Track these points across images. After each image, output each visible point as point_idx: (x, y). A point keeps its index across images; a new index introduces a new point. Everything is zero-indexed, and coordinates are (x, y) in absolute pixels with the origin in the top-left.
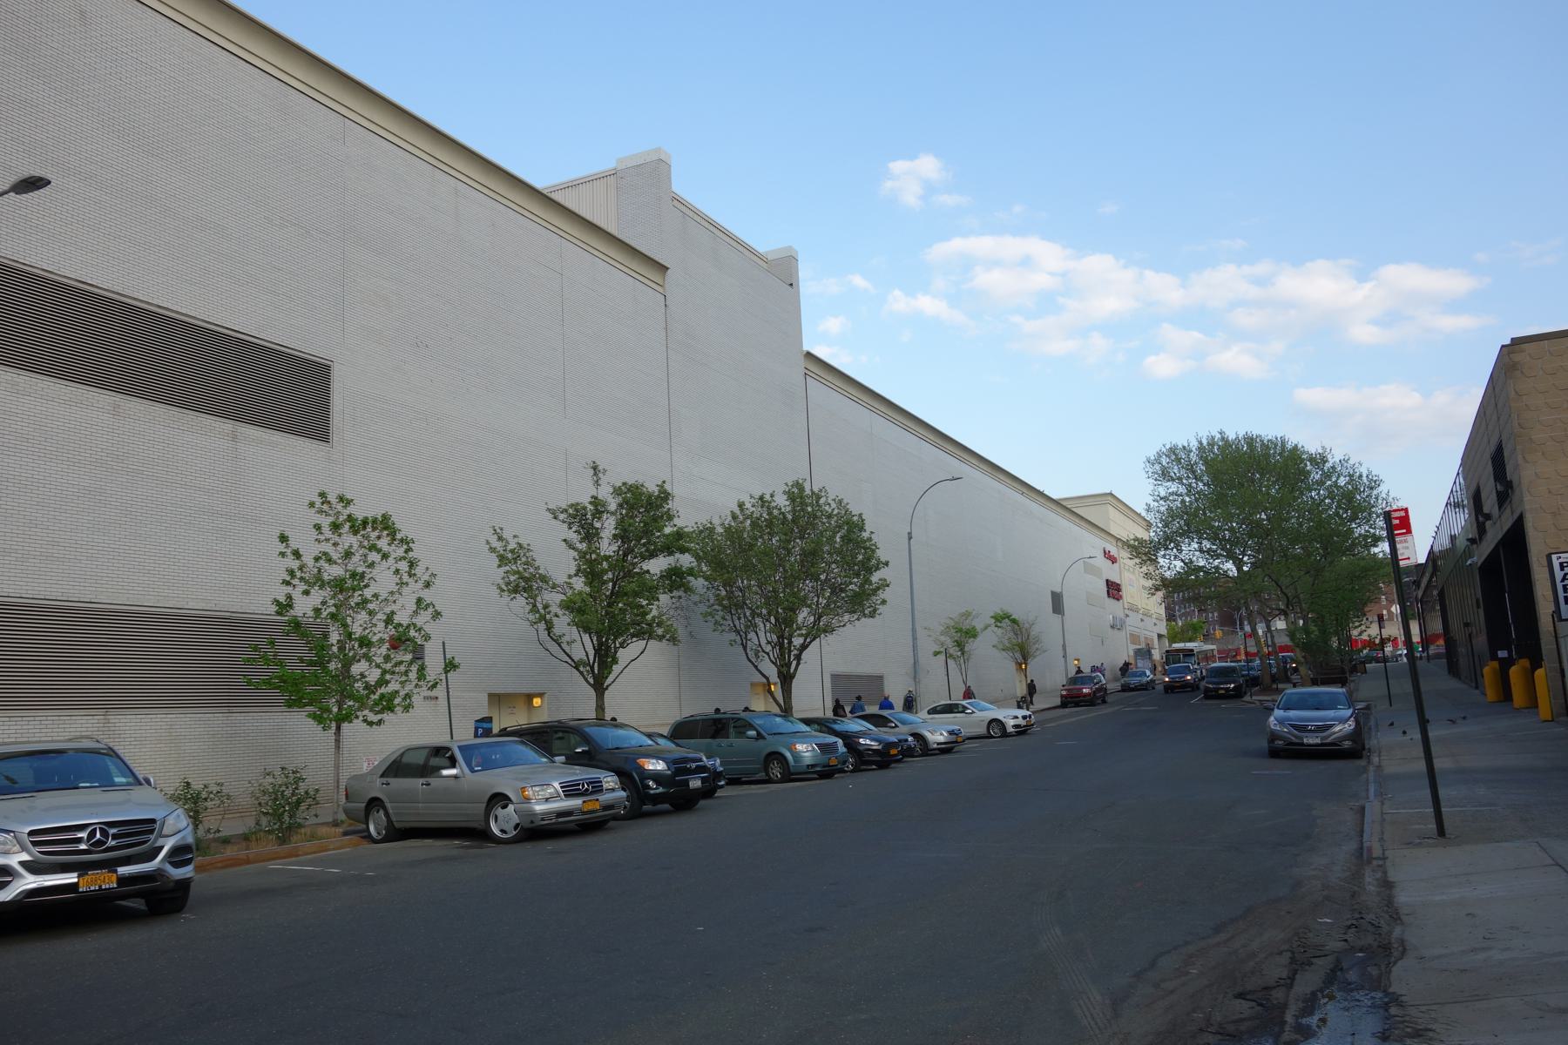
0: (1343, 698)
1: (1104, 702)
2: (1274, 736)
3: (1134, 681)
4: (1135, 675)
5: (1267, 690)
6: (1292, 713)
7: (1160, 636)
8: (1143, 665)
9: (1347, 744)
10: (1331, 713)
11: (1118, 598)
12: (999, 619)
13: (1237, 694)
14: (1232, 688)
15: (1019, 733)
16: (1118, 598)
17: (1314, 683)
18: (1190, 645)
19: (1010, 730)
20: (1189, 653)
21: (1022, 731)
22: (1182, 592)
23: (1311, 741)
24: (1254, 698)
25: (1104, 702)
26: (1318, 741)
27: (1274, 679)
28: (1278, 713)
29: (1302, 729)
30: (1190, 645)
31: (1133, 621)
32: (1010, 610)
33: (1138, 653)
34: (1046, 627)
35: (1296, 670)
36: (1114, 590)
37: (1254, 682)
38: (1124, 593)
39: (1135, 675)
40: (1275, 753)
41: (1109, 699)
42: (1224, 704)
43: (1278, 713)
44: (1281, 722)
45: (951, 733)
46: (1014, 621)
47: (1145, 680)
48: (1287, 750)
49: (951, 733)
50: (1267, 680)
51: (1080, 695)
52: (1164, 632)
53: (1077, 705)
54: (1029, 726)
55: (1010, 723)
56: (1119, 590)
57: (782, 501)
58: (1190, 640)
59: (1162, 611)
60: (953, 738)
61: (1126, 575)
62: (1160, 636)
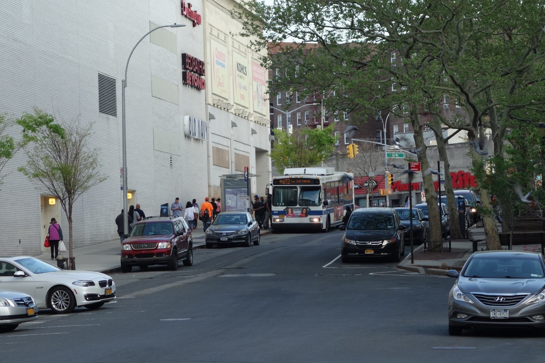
0: (538, 264)
1: (187, 263)
2: (457, 309)
3: (227, 230)
4: (228, 220)
5: (436, 251)
6: (479, 282)
7: (260, 152)
8: (238, 204)
9: (538, 319)
10: (524, 283)
11: (199, 86)
12: (31, 124)
13: (392, 256)
14: (377, 246)
15: (90, 308)
16: (199, 86)
17: (505, 241)
18: (313, 172)
19: (82, 301)
20: (312, 185)
21: (96, 304)
22: (294, 76)
23: (499, 315)
24: (416, 263)
25: (187, 263)
26: (506, 315)
27: (446, 234)
28: (463, 281)
29: (489, 300)
30: (313, 172)
31: (220, 125)
32: (48, 110)
33: (229, 182)
34: (100, 138)
35: (476, 218)
36: (193, 71)
37: (415, 237)
38: (208, 77)
39: (228, 220)
40: (456, 330)
41: (195, 259)
42: (373, 272)
43: (463, 281)
44: (465, 292)
45: (19, 302)
46: (56, 130)
47: (244, 229)
48: (470, 326)
49: (19, 302)
50: (436, 234)
51: (147, 250)
52: (266, 146)
53: (144, 268)
54: (108, 296)
55: (82, 293)
56: (201, 72)
57: (348, 151)
58: (312, 162)
59: (265, 109)
60: (22, 310)
61: (214, 46)
62: (260, 152)
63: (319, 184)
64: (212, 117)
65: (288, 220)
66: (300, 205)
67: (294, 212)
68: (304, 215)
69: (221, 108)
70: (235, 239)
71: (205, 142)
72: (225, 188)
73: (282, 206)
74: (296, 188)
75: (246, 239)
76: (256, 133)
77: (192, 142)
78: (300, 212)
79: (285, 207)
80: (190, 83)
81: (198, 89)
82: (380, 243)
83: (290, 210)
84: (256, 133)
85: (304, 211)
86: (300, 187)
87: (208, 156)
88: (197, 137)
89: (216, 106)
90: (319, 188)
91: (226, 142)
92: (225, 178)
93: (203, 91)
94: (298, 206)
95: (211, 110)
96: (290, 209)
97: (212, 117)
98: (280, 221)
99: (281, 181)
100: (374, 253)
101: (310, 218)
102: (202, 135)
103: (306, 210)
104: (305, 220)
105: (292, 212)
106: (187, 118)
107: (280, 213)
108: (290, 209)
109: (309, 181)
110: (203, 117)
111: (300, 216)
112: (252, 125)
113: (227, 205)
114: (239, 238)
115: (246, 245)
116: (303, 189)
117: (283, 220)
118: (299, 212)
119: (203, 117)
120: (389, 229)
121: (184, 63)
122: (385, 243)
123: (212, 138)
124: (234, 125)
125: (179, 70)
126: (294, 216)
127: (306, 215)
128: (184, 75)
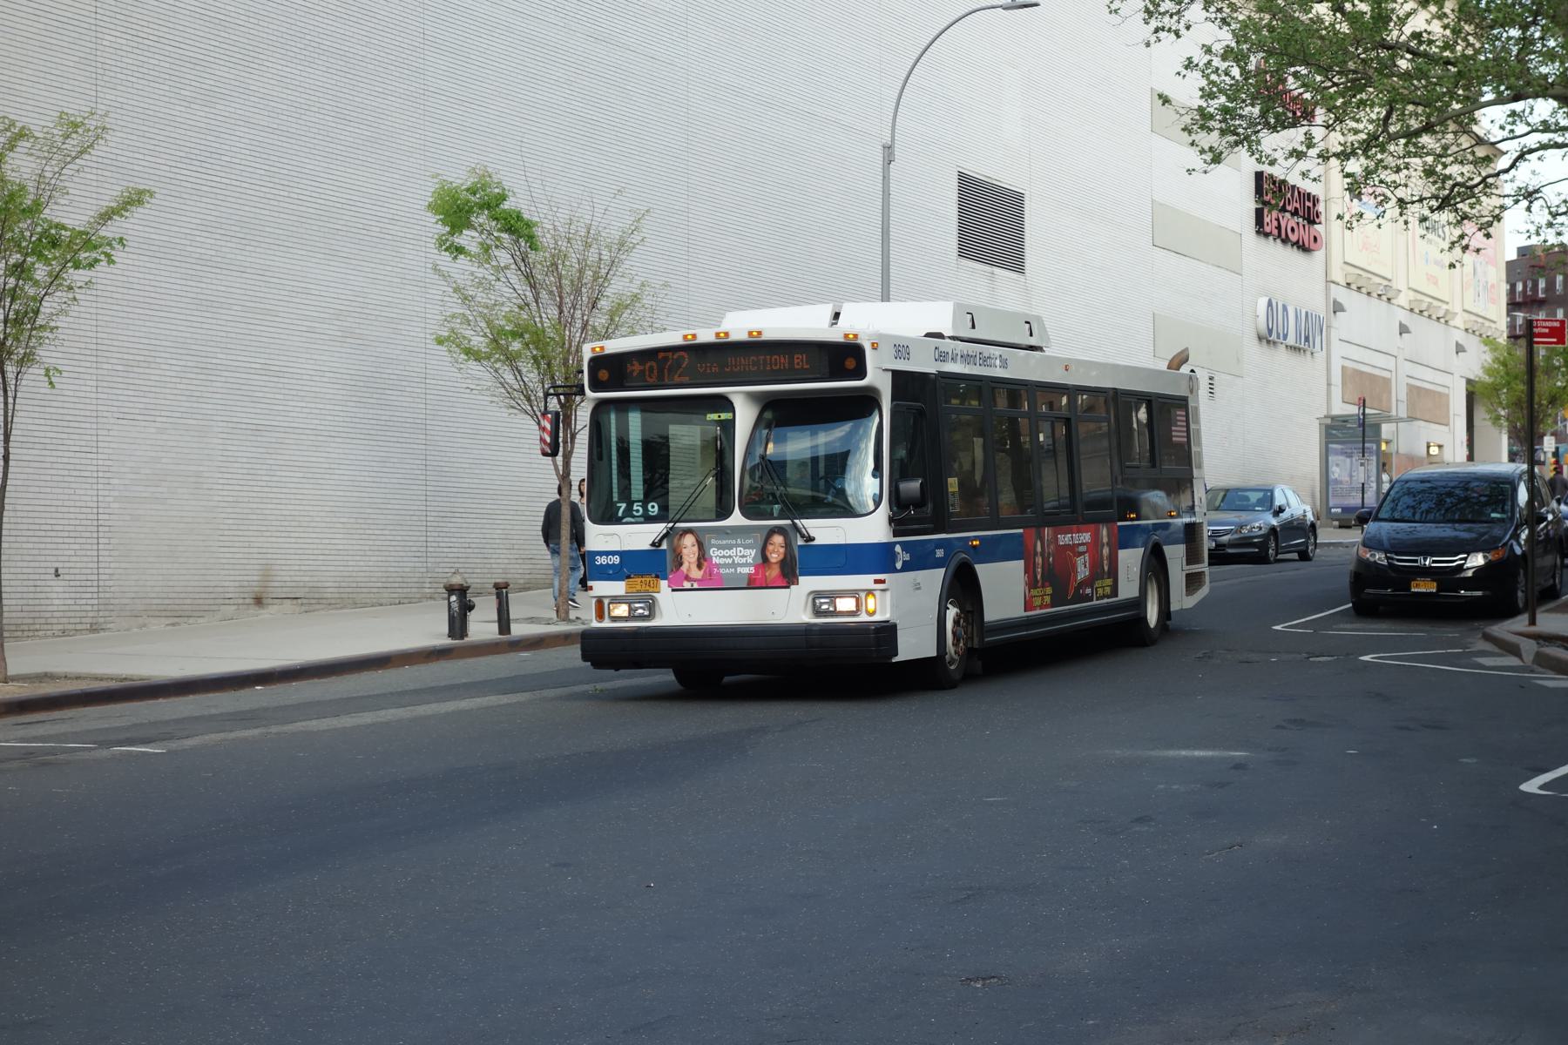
56: (1312, 219)
63: (860, 372)
64: (1338, 308)
65: (680, 609)
66: (746, 514)
67: (716, 555)
68: (774, 572)
69: (1369, 294)
70: (1232, 545)
71: (1320, 356)
72: (1327, 443)
73: (649, 519)
74: (724, 403)
75: (1263, 546)
76: (1408, 331)
77: (1281, 354)
78: (751, 555)
79: (659, 528)
80: (1275, 232)
81: (1303, 248)
82: (1457, 560)
83: (688, 544)
84: (1408, 331)
85: (776, 554)
86: (753, 396)
87: (1329, 385)
88: (1291, 340)
89: (1354, 287)
90: (864, 403)
91: (1380, 360)
92: (1329, 421)
93: (1319, 255)
94: (736, 519)
96: (689, 540)
97: (1338, 308)
98: (631, 617)
99: (636, 367)
100: (1439, 590)
101: (817, 595)
102: (1307, 339)
103: (788, 545)
104: (787, 607)
105: (702, 559)
106: (1263, 302)
107: (632, 565)
108: (689, 540)
109: (800, 360)
110: (1319, 307)
111: (753, 584)
112: (1459, 336)
113: (1332, 477)
114: (1246, 542)
115: (1260, 558)
116: (781, 414)
117: (652, 607)
118: (739, 557)
119: (1319, 307)
120: (1494, 521)
121: (1259, 190)
122: (1478, 560)
124: (1404, 329)
125: (1250, 205)
126: (713, 582)
127: (789, 574)
128: (1259, 215)
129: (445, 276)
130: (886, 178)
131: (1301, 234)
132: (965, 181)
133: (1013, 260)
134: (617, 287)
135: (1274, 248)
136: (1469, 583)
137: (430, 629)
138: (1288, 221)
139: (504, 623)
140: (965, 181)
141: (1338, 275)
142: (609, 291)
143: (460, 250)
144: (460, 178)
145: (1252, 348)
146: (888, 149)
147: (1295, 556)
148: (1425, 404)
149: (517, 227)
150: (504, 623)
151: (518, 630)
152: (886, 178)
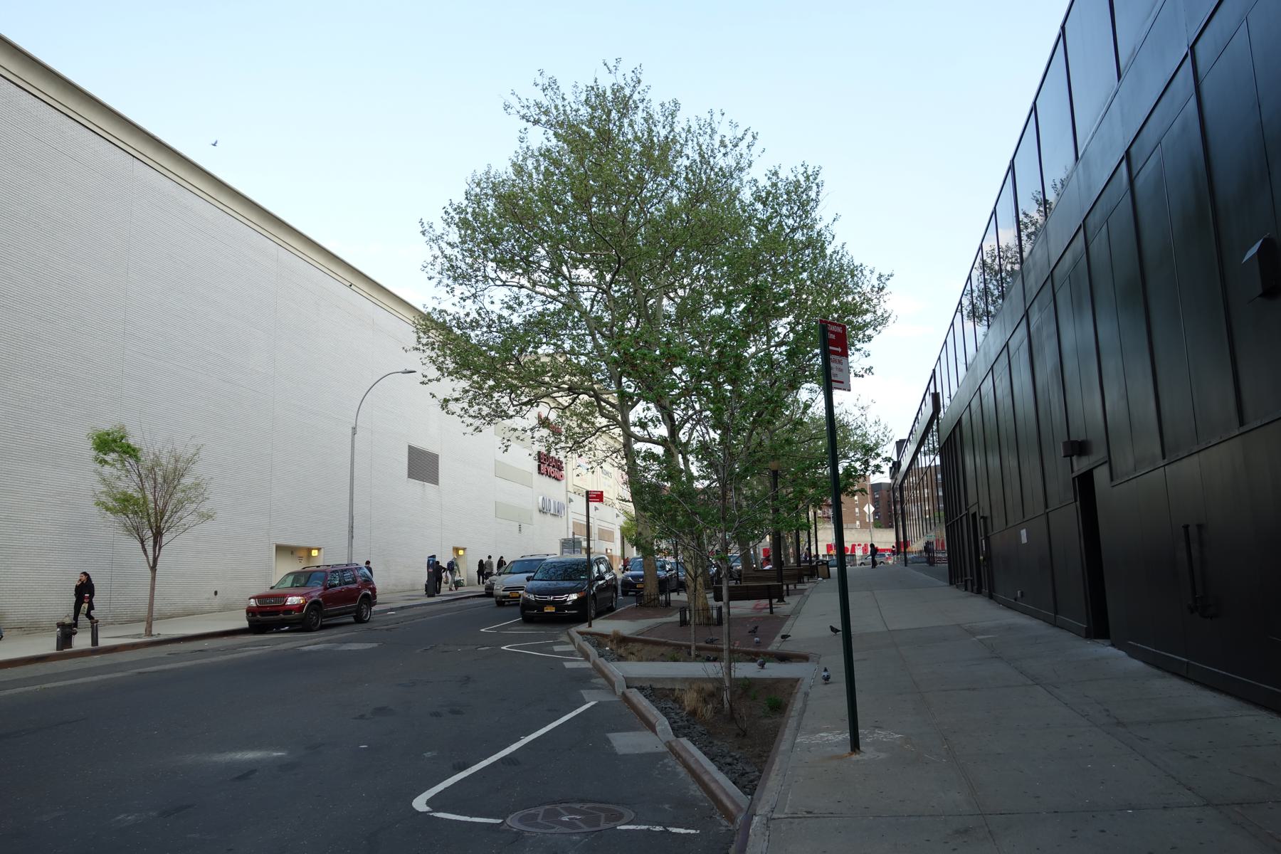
56: (560, 469)
64: (571, 501)
93: (563, 482)
95: (572, 496)
97: (571, 501)
110: (563, 500)
122: (574, 597)
123: (571, 516)
129: (100, 474)
130: (353, 441)
131: (557, 474)
132: (410, 447)
133: (434, 479)
134: (187, 481)
135: (545, 479)
136: (569, 608)
137: (48, 645)
138: (551, 469)
139: (95, 641)
140: (410, 447)
141: (571, 489)
142: (183, 481)
143: (106, 462)
144: (106, 426)
145: (537, 515)
146: (354, 429)
147: (352, 620)
148: (605, 535)
149: (130, 452)
150: (95, 641)
151: (103, 642)
152: (353, 441)
